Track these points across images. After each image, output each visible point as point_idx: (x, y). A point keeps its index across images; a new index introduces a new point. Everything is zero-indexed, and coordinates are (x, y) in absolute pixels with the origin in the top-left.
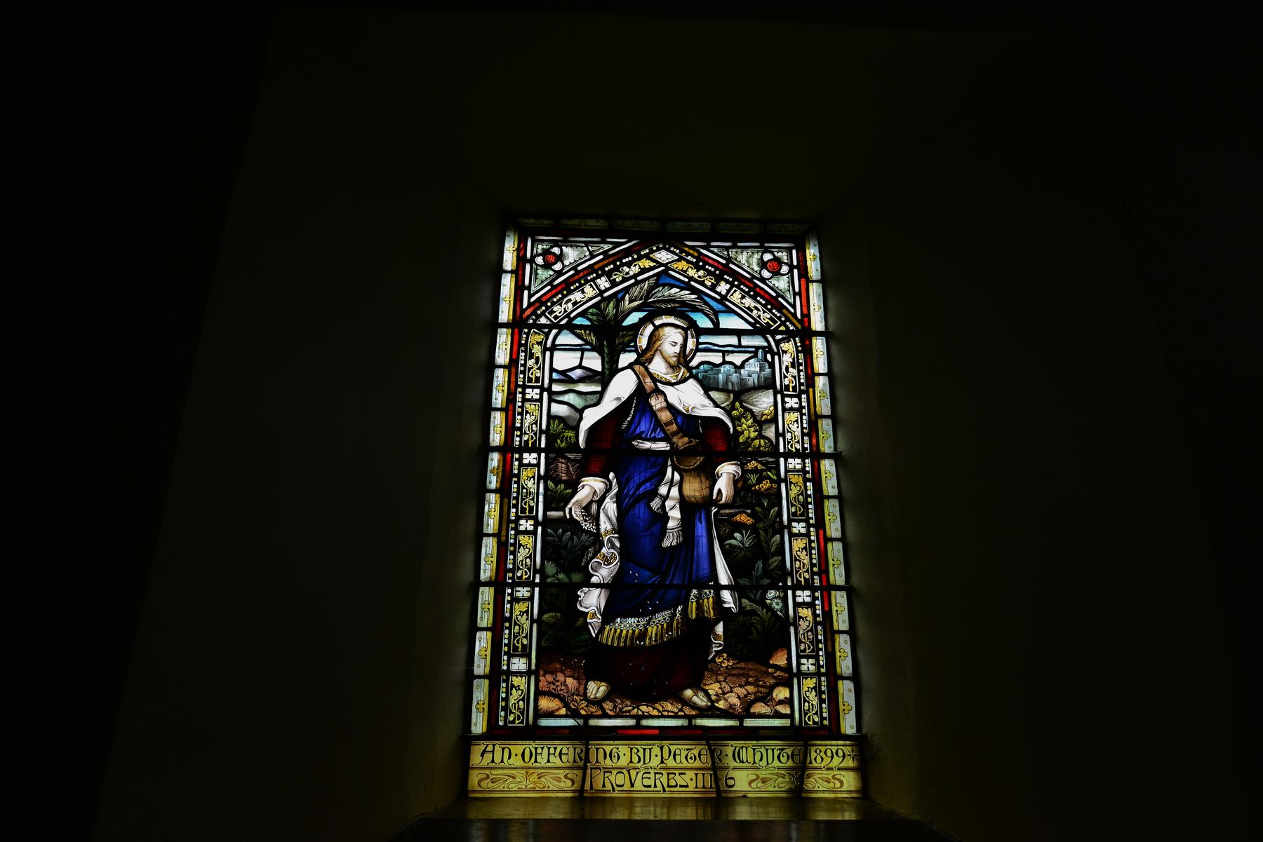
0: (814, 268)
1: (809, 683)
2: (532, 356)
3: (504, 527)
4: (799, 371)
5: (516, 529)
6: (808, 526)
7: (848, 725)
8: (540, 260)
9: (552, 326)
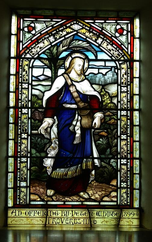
2: (24, 71)
4: (128, 76)
5: (21, 137)
6: (127, 136)
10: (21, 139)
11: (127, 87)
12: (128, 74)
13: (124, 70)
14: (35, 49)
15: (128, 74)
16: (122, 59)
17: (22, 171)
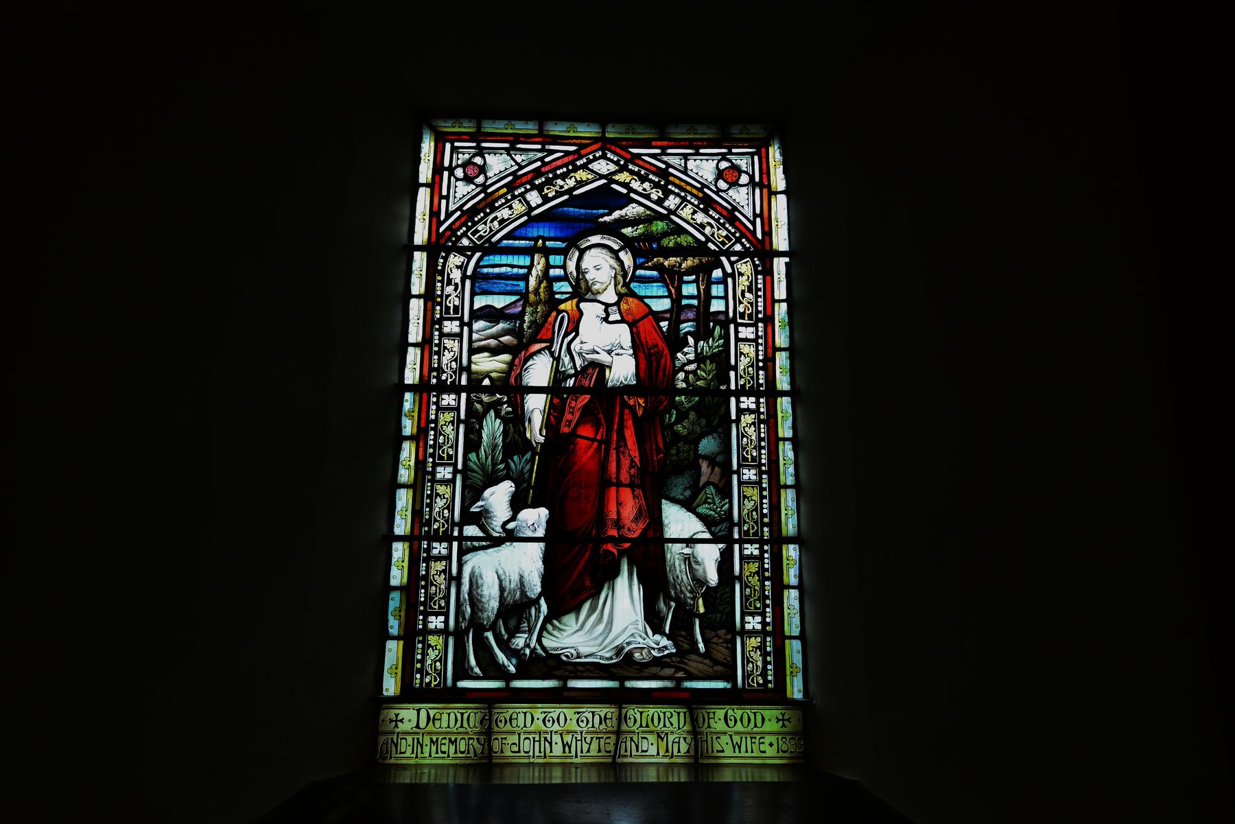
0: (779, 181)
1: (754, 642)
2: (449, 282)
3: (420, 477)
4: (757, 297)
5: (440, 330)
6: (761, 473)
7: (795, 689)
8: (459, 173)
9: (474, 249)
10: (437, 410)
11: (755, 325)
12: (758, 290)
13: (745, 277)
14: (485, 223)
15: (758, 290)
16: (738, 247)
17: (432, 584)
